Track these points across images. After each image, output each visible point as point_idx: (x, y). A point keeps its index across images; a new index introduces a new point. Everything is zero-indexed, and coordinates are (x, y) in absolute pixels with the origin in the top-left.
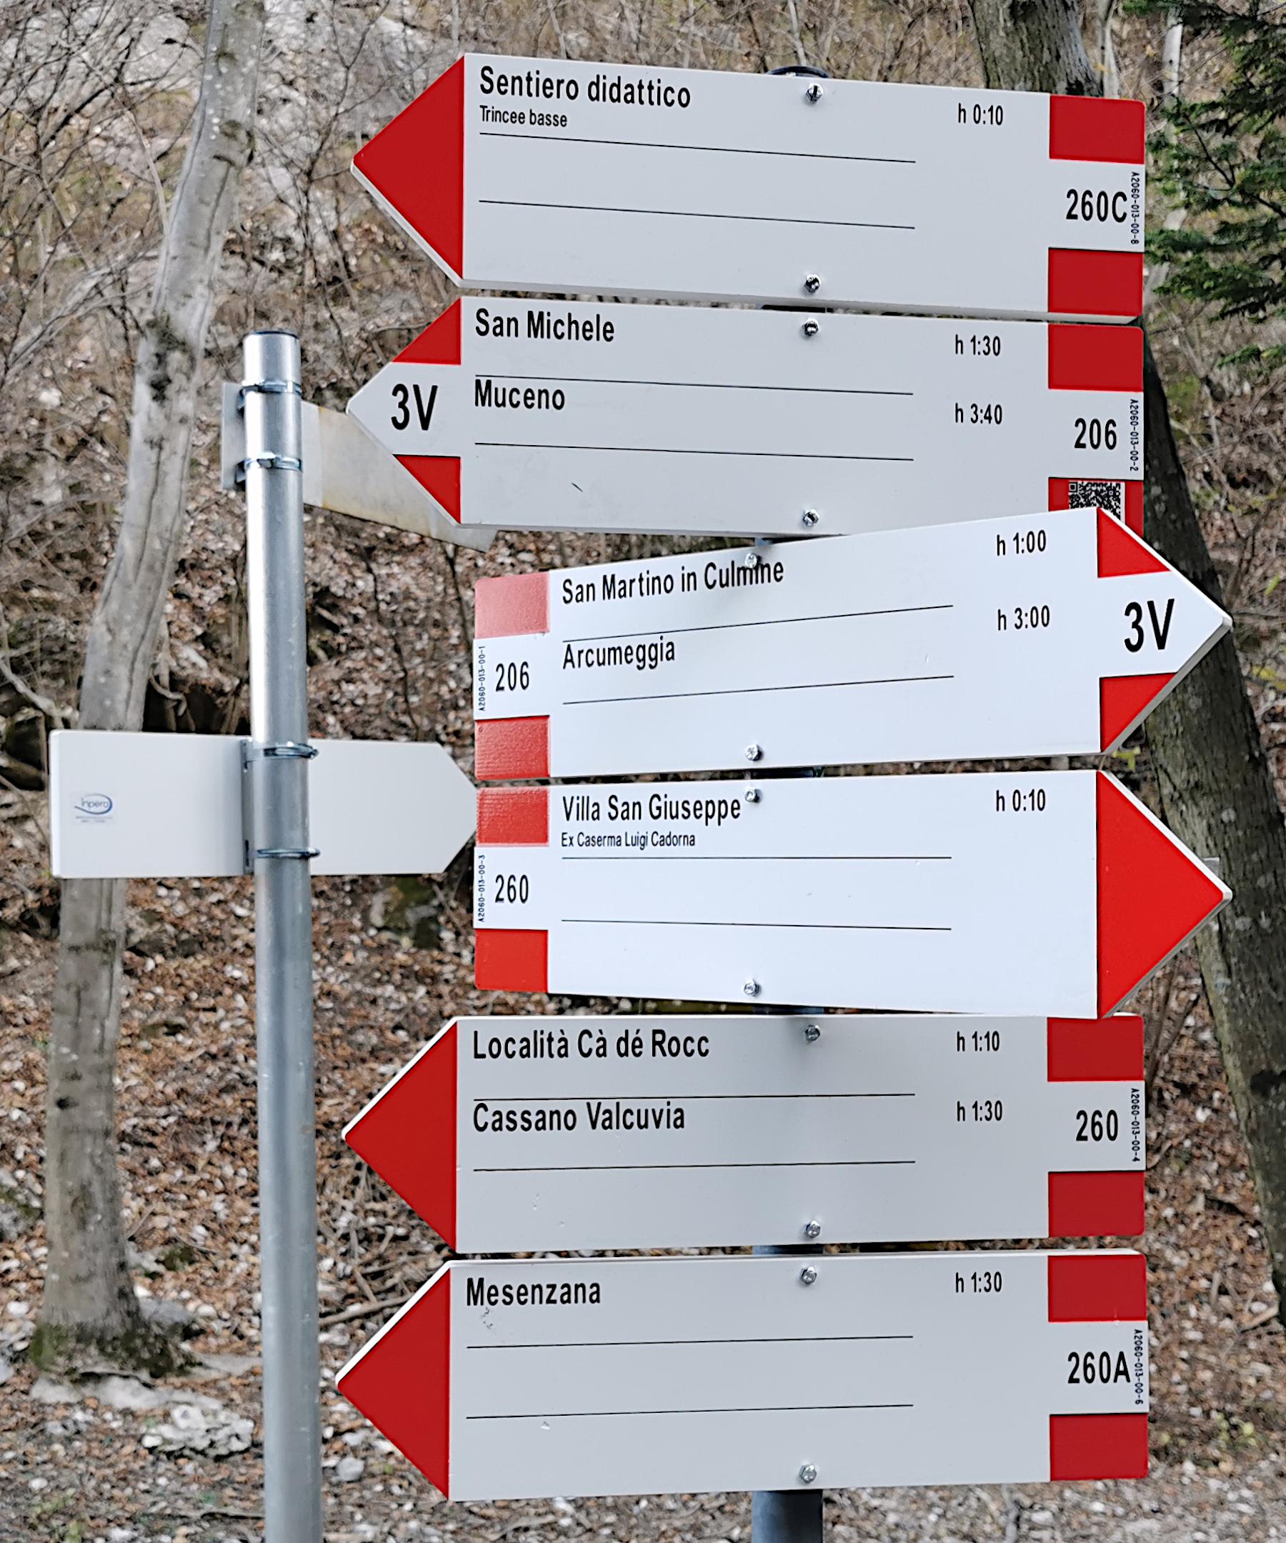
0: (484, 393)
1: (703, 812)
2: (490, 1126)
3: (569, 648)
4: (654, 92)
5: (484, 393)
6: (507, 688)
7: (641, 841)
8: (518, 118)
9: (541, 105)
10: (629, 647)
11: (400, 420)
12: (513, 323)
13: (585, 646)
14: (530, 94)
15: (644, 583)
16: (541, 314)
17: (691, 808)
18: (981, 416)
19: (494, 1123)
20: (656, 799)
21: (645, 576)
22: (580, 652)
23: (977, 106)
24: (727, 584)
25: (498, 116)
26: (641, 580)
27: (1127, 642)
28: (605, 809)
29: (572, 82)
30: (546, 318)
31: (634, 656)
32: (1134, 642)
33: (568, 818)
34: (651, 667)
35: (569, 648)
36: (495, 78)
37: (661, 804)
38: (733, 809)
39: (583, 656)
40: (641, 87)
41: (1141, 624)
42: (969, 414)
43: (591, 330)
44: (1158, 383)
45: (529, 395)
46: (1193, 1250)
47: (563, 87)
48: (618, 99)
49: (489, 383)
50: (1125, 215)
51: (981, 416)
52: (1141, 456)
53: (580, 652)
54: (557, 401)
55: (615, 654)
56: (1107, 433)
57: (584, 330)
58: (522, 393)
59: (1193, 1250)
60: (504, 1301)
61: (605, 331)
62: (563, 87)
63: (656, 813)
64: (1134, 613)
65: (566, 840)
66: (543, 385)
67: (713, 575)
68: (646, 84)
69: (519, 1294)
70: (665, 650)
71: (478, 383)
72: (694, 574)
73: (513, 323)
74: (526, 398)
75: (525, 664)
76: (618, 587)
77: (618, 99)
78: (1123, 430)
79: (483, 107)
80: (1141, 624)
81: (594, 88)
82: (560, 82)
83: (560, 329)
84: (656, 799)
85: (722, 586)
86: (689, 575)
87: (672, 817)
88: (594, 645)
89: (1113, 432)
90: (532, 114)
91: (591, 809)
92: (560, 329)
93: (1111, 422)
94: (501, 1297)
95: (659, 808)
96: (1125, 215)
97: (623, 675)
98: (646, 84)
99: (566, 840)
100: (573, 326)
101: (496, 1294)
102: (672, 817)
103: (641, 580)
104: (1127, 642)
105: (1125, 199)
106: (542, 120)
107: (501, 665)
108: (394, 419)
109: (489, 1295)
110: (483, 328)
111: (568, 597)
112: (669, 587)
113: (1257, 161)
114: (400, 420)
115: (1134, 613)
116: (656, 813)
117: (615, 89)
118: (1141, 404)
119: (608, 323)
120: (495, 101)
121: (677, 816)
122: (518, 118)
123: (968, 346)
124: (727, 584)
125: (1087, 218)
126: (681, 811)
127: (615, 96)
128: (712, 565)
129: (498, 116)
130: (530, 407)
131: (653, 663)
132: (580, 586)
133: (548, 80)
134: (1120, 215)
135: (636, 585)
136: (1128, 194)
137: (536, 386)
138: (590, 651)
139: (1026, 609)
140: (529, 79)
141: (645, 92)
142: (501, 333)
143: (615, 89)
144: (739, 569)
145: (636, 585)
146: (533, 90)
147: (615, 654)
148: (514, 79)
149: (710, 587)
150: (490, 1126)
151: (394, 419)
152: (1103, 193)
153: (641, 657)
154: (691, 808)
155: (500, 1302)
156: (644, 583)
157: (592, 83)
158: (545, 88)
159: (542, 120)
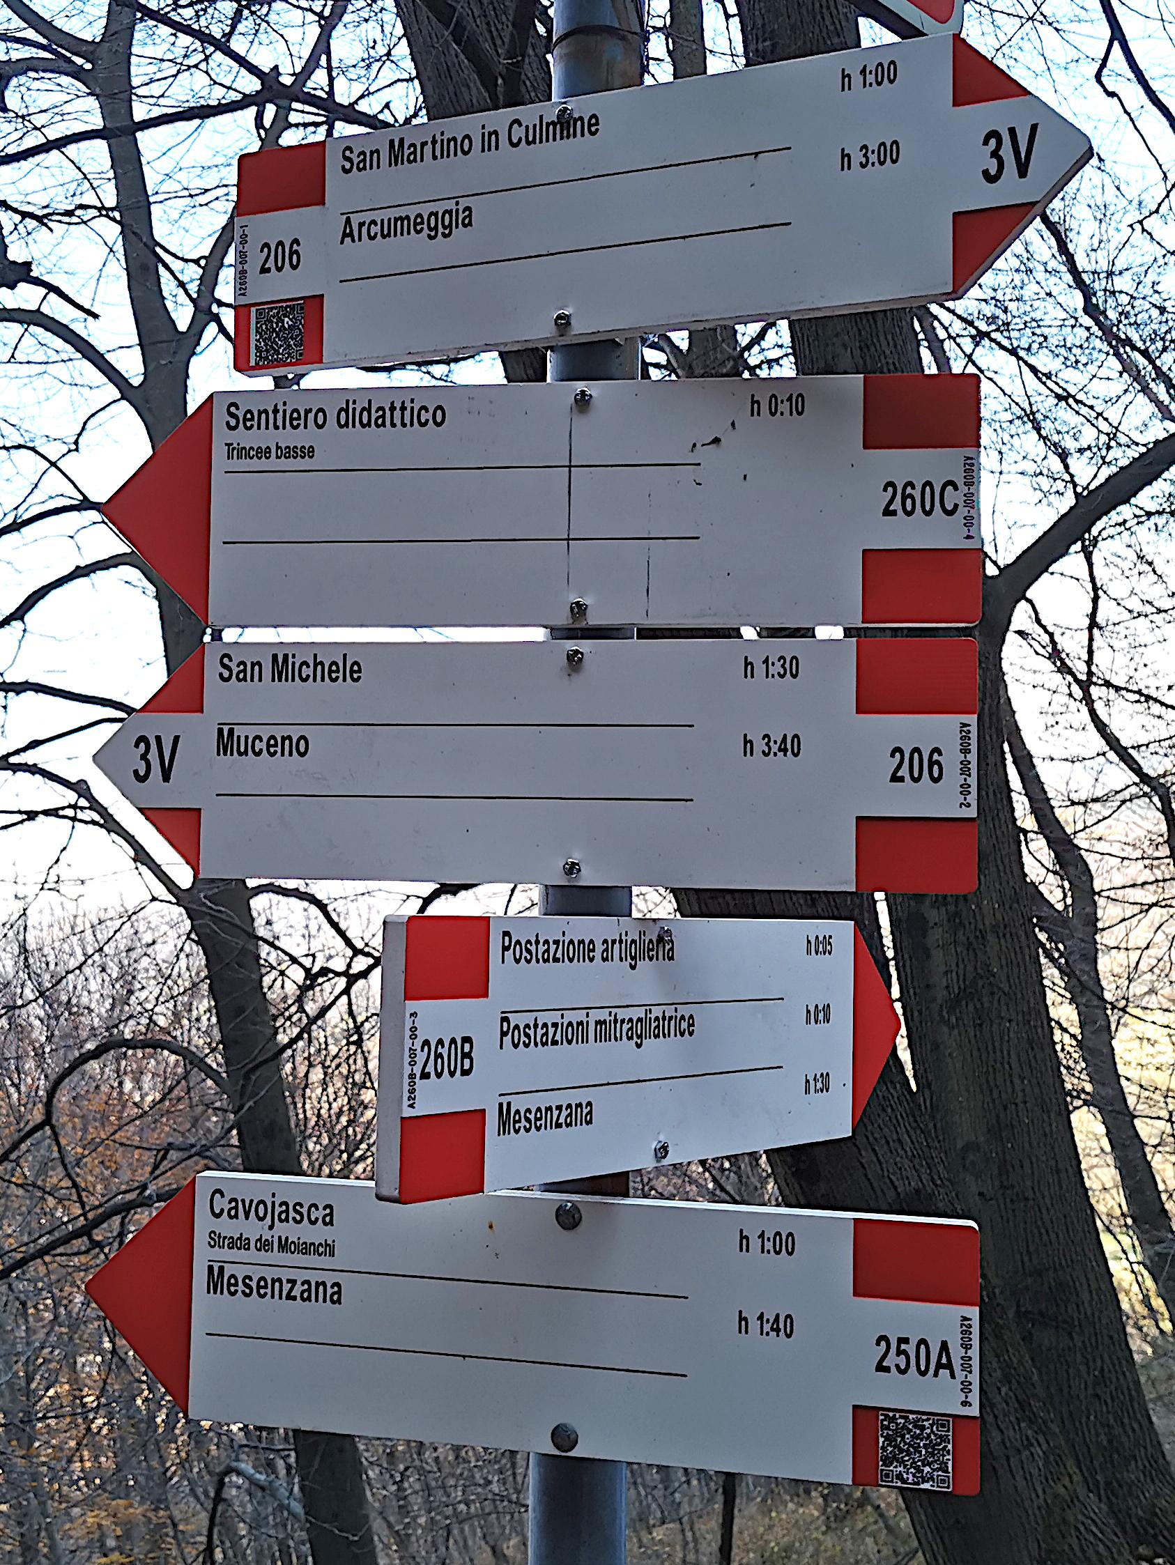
0: (226, 742)
2: (225, 1213)
3: (348, 221)
4: (407, 413)
5: (226, 742)
8: (263, 453)
9: (288, 437)
10: (419, 215)
11: (142, 773)
12: (257, 668)
13: (367, 217)
14: (276, 427)
15: (438, 146)
18: (775, 748)
19: (230, 1210)
21: (438, 138)
23: (774, 396)
24: (534, 142)
25: (243, 453)
26: (434, 142)
29: (321, 410)
31: (425, 226)
32: (993, 172)
34: (444, 235)
35: (348, 221)
36: (240, 415)
39: (364, 230)
40: (393, 409)
42: (760, 746)
43: (338, 671)
45: (272, 742)
47: (311, 416)
48: (369, 424)
49: (231, 732)
50: (956, 506)
51: (775, 748)
52: (974, 789)
53: (361, 225)
54: (300, 747)
55: (403, 225)
56: (932, 763)
57: (330, 672)
58: (265, 740)
60: (243, 1292)
61: (352, 671)
62: (311, 416)
64: (993, 142)
66: (286, 731)
67: (518, 132)
68: (398, 405)
69: (259, 1287)
71: (220, 731)
72: (495, 132)
73: (257, 668)
74: (269, 746)
75: (296, 241)
76: (407, 152)
77: (369, 424)
78: (951, 760)
79: (228, 445)
81: (343, 414)
82: (308, 412)
85: (528, 143)
86: (490, 134)
89: (938, 763)
90: (278, 447)
92: (305, 670)
93: (937, 750)
94: (241, 1287)
96: (956, 506)
97: (413, 248)
98: (398, 405)
100: (319, 667)
101: (236, 1284)
105: (956, 488)
106: (289, 452)
107: (266, 245)
108: (136, 772)
109: (229, 1285)
110: (226, 674)
111: (348, 166)
114: (142, 773)
117: (365, 413)
118: (974, 729)
119: (356, 663)
120: (243, 438)
122: (263, 453)
123: (760, 669)
124: (534, 142)
125: (909, 514)
127: (365, 421)
128: (517, 122)
129: (243, 453)
130: (272, 755)
133: (296, 410)
134: (949, 507)
135: (428, 149)
136: (960, 484)
137: (279, 732)
138: (374, 222)
139: (873, 146)
140: (276, 411)
141: (397, 413)
142: (245, 679)
143: (365, 413)
144: (548, 125)
145: (428, 149)
146: (280, 423)
147: (403, 225)
148: (260, 413)
149: (514, 145)
150: (225, 1213)
151: (136, 772)
152: (928, 483)
155: (240, 1293)
156: (438, 146)
157: (341, 409)
158: (292, 419)
159: (289, 452)
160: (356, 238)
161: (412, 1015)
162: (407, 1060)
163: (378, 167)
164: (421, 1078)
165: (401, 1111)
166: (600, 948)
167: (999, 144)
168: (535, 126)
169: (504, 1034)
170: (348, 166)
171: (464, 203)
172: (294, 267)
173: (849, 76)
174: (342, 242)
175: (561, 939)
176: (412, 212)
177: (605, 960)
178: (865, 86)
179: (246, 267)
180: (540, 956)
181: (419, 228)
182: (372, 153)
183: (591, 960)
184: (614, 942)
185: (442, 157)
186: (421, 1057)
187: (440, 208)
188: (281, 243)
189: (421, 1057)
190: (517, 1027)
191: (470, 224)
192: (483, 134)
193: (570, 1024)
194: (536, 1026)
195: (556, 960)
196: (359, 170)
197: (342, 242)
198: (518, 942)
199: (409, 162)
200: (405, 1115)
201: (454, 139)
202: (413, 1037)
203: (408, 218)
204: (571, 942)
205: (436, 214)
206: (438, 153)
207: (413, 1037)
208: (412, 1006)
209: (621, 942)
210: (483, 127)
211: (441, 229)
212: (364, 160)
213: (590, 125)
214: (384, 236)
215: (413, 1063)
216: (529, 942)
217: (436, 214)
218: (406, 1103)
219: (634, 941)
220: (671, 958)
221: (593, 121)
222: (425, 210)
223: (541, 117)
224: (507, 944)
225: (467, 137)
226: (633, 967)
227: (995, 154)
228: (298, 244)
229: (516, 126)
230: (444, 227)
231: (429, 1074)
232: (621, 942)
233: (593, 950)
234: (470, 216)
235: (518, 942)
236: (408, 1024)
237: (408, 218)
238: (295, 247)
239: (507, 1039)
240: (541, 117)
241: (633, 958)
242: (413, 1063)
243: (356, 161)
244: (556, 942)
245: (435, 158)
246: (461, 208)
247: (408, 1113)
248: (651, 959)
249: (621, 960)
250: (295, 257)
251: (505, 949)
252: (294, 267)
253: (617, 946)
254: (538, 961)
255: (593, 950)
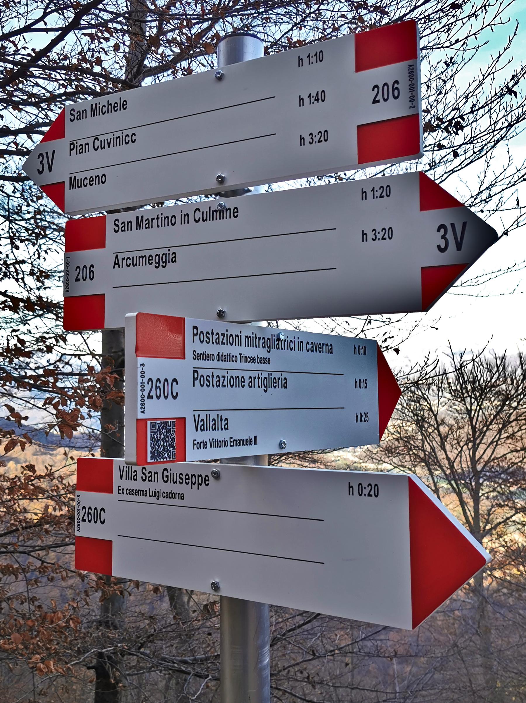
1: (190, 481)
3: (117, 256)
6: (81, 280)
7: (157, 494)
10: (151, 256)
13: (126, 255)
16: (96, 104)
17: (183, 478)
20: (165, 472)
21: (160, 216)
22: (123, 259)
24: (206, 220)
26: (158, 218)
27: (439, 247)
28: (140, 475)
30: (98, 106)
31: (153, 261)
32: (443, 246)
33: (121, 478)
34: (163, 266)
35: (117, 256)
37: (168, 474)
38: (205, 480)
39: (125, 261)
41: (447, 236)
44: (430, 474)
46: (465, 396)
53: (123, 259)
59: (465, 396)
63: (166, 479)
64: (442, 230)
65: (121, 491)
67: (198, 215)
70: (171, 257)
72: (187, 215)
74: (90, 181)
75: (92, 266)
76: (145, 223)
80: (447, 236)
83: (105, 109)
84: (165, 472)
85: (204, 221)
86: (185, 215)
87: (174, 483)
88: (131, 255)
91: (133, 474)
92: (105, 109)
95: (167, 476)
99: (121, 491)
102: (174, 483)
103: (158, 218)
104: (439, 247)
111: (117, 229)
112: (173, 222)
113: (454, 666)
115: (442, 230)
116: (166, 479)
121: (176, 482)
124: (206, 220)
126: (178, 479)
131: (164, 265)
132: (124, 223)
138: (129, 258)
139: (379, 229)
144: (213, 212)
145: (155, 221)
153: (157, 261)
154: (183, 478)
156: (160, 220)
160: (121, 266)
161: (141, 365)
162: (139, 388)
163: (131, 230)
164: (148, 398)
165: (137, 415)
166: (247, 381)
167: (446, 232)
168: (207, 212)
169: (195, 379)
170: (117, 229)
171: (172, 250)
172: (91, 279)
173: (365, 192)
174: (114, 268)
175: (226, 333)
176: (147, 253)
177: (251, 387)
178: (374, 198)
179: (69, 277)
180: (215, 384)
181: (150, 262)
182: (128, 223)
183: (243, 387)
184: (255, 378)
185: (162, 226)
186: (147, 387)
187: (161, 252)
188: (85, 267)
189: (147, 387)
190: (202, 376)
191: (175, 261)
192: (182, 215)
193: (232, 377)
194: (213, 376)
195: (224, 386)
196: (122, 231)
197: (114, 268)
198: (202, 332)
199: (146, 228)
200: (139, 418)
201: (168, 217)
202: (143, 376)
203: (145, 256)
204: (231, 335)
205: (159, 255)
206: (160, 224)
207: (143, 376)
208: (141, 360)
209: (259, 378)
210: (182, 212)
211: (161, 263)
212: (124, 226)
213: (234, 213)
214: (134, 265)
215: (143, 390)
216: (208, 333)
217: (159, 255)
218: (139, 410)
219: (265, 378)
220: (286, 387)
221: (236, 210)
222: (154, 253)
223: (210, 207)
224: (195, 332)
225: (174, 216)
226: (266, 391)
227: (443, 237)
228: (93, 268)
229: (197, 211)
230: (163, 262)
231: (152, 396)
232: (259, 378)
233: (244, 382)
234: (175, 257)
235: (202, 332)
236: (140, 370)
237: (145, 256)
238: (92, 269)
239: (197, 382)
240: (210, 207)
241: (266, 387)
242: (143, 390)
243: (120, 226)
244: (223, 335)
245: (158, 226)
246: (171, 252)
247: (140, 416)
248: (275, 387)
249: (259, 387)
250: (92, 274)
251: (194, 335)
252: (91, 279)
253: (256, 380)
254: (213, 386)
255: (244, 382)
